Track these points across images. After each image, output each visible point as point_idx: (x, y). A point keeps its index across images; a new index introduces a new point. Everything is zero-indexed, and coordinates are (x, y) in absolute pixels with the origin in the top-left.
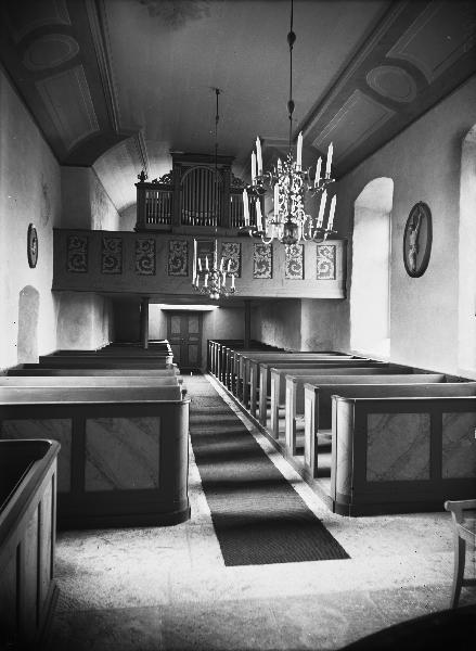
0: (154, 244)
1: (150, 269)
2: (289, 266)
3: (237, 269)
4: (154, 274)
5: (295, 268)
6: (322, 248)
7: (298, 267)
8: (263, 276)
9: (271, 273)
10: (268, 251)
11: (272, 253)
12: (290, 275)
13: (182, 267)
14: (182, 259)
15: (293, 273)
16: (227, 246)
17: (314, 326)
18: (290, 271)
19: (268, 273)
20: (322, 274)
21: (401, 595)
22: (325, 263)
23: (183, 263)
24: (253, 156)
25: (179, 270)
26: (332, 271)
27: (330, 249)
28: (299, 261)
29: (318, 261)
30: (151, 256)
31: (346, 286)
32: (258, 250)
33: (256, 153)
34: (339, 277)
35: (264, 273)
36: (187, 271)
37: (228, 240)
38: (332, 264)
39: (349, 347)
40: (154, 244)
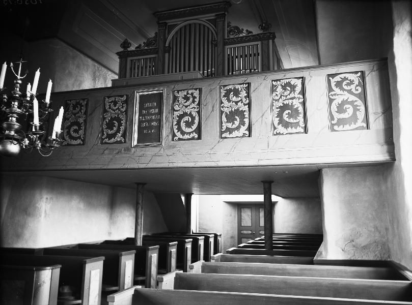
0: (87, 104)
1: (79, 138)
2: (280, 115)
3: (194, 127)
4: (199, 138)
5: (290, 116)
6: (338, 78)
7: (292, 115)
8: (235, 134)
9: (249, 129)
10: (244, 94)
11: (248, 96)
12: (281, 129)
13: (118, 131)
14: (119, 120)
15: (286, 125)
16: (181, 95)
17: (351, 213)
18: (281, 122)
19: (243, 129)
20: (341, 122)
21: (100, 283)
22: (344, 102)
23: (120, 125)
24: (29, 86)
25: (114, 135)
26: (361, 115)
27: (355, 78)
28: (297, 104)
29: (331, 101)
30: (81, 120)
31: (390, 138)
32: (227, 95)
33: (32, 85)
34: (377, 123)
35: (238, 128)
36: (124, 135)
37: (178, 87)
38: (360, 103)
39: (352, 230)
40: (87, 104)
